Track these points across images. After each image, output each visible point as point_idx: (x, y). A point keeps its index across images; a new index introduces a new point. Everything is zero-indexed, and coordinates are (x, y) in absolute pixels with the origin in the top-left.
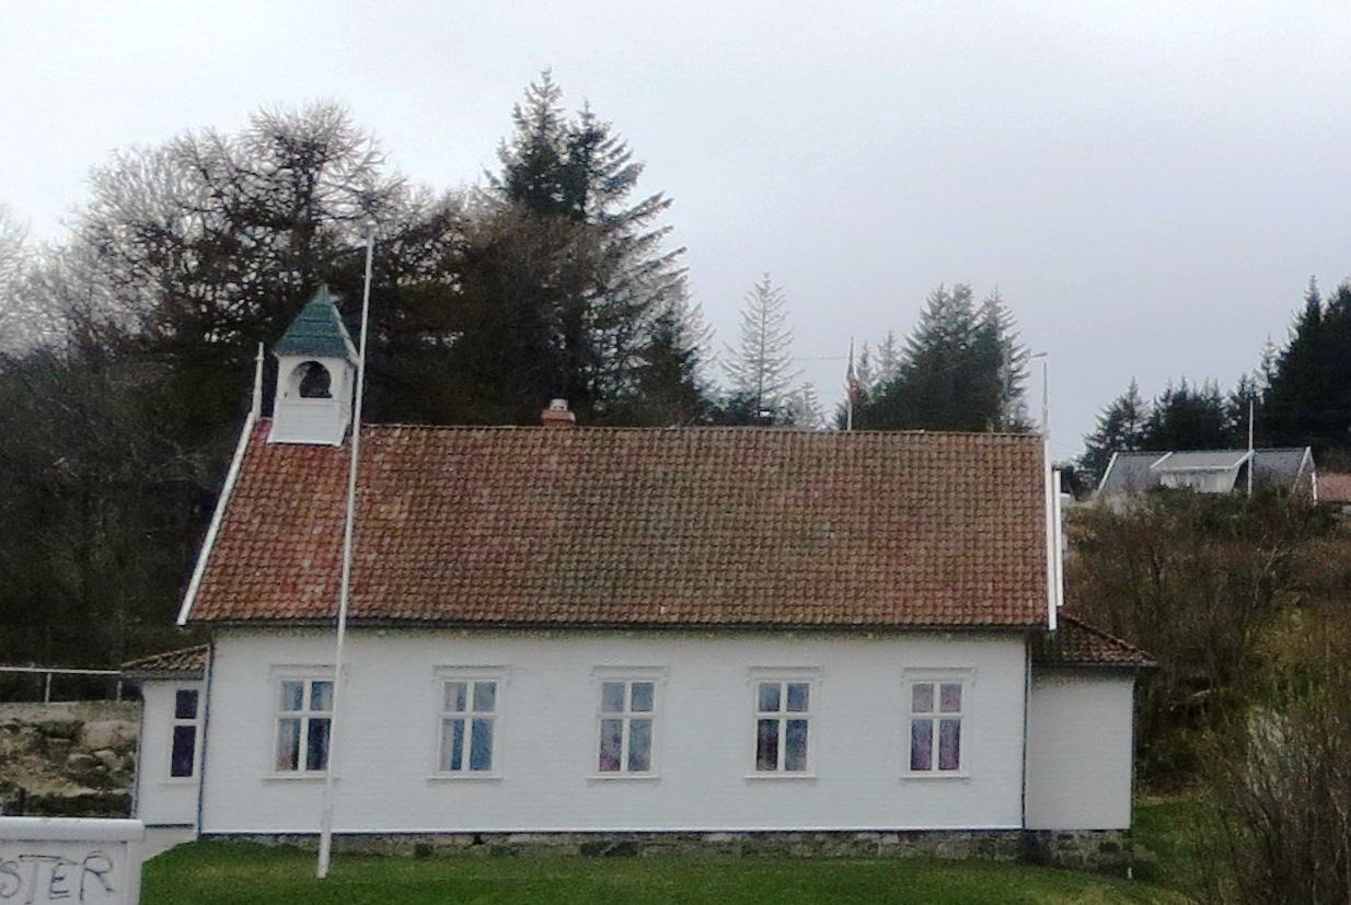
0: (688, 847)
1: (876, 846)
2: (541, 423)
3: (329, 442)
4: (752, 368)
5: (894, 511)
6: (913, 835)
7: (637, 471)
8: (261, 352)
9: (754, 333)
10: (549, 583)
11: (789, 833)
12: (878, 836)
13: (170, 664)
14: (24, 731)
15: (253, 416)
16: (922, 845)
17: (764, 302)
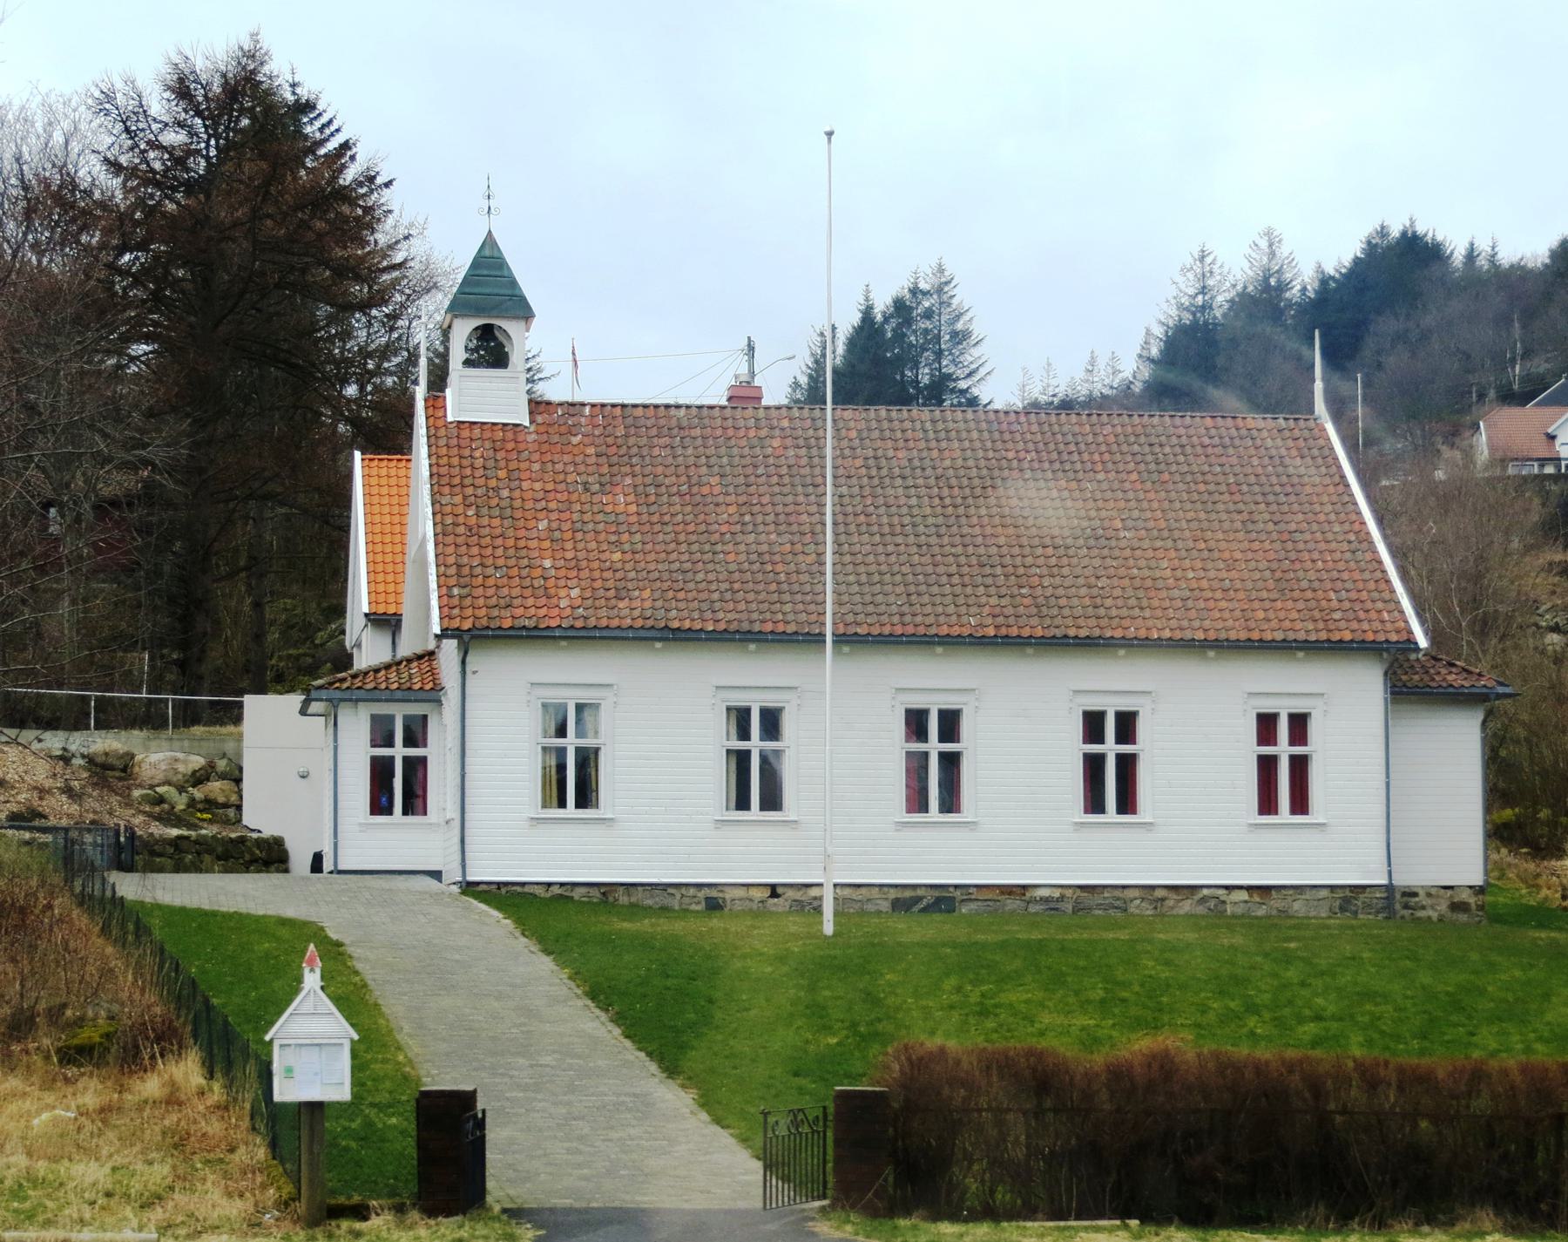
0: (1012, 904)
1: (1224, 902)
3: (518, 422)
6: (1265, 890)
11: (1124, 887)
12: (1224, 892)
16: (1276, 902)
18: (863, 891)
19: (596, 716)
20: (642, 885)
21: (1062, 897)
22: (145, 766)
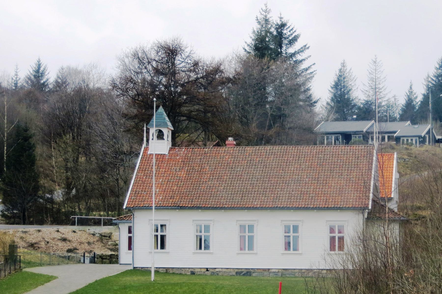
0: (266, 273)
2: (226, 145)
4: (372, 91)
5: (326, 171)
7: (251, 160)
8: (145, 127)
9: (372, 78)
10: (224, 195)
11: (294, 269)
13: (126, 218)
14: (97, 235)
15: (144, 145)
17: (375, 66)
18: (229, 270)
19: (102, 233)
20: (176, 268)
21: (278, 272)
22: (115, 236)
